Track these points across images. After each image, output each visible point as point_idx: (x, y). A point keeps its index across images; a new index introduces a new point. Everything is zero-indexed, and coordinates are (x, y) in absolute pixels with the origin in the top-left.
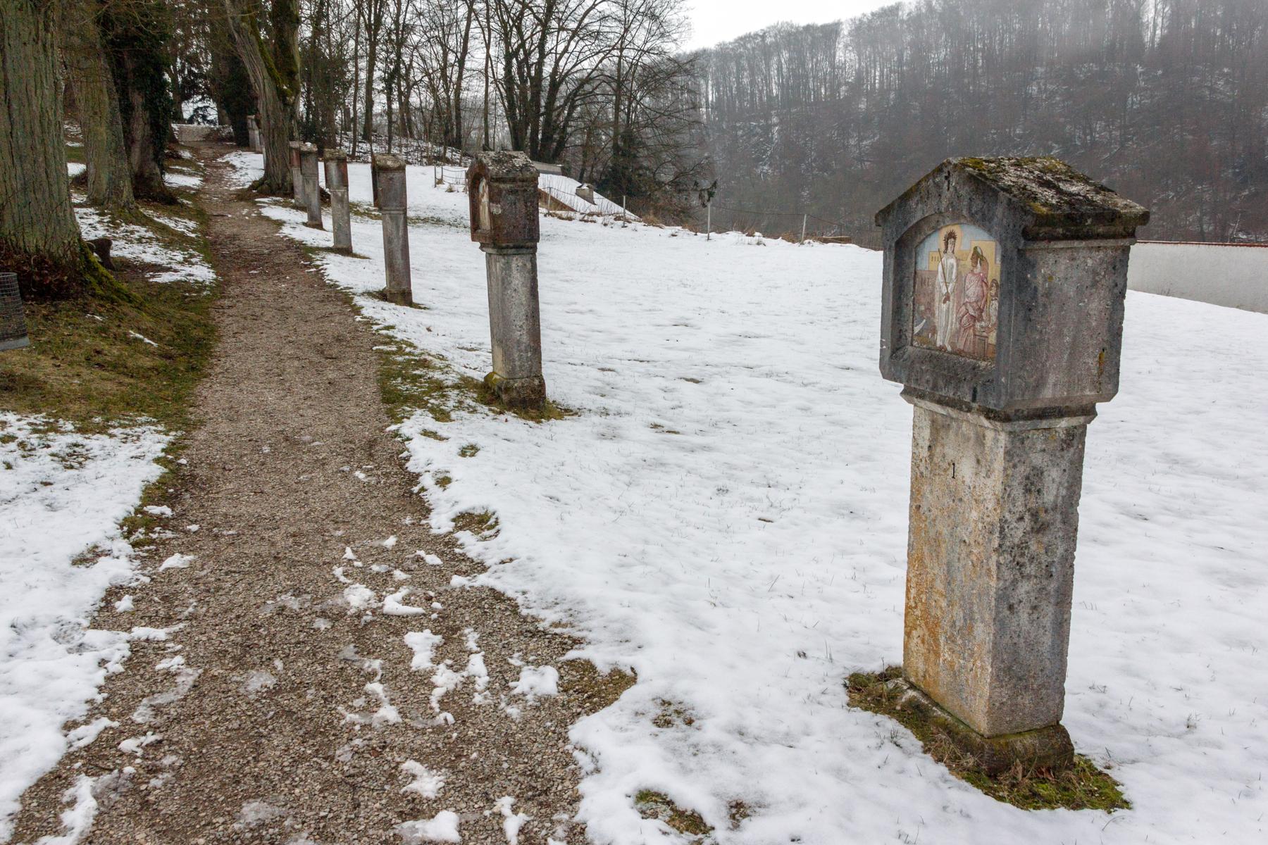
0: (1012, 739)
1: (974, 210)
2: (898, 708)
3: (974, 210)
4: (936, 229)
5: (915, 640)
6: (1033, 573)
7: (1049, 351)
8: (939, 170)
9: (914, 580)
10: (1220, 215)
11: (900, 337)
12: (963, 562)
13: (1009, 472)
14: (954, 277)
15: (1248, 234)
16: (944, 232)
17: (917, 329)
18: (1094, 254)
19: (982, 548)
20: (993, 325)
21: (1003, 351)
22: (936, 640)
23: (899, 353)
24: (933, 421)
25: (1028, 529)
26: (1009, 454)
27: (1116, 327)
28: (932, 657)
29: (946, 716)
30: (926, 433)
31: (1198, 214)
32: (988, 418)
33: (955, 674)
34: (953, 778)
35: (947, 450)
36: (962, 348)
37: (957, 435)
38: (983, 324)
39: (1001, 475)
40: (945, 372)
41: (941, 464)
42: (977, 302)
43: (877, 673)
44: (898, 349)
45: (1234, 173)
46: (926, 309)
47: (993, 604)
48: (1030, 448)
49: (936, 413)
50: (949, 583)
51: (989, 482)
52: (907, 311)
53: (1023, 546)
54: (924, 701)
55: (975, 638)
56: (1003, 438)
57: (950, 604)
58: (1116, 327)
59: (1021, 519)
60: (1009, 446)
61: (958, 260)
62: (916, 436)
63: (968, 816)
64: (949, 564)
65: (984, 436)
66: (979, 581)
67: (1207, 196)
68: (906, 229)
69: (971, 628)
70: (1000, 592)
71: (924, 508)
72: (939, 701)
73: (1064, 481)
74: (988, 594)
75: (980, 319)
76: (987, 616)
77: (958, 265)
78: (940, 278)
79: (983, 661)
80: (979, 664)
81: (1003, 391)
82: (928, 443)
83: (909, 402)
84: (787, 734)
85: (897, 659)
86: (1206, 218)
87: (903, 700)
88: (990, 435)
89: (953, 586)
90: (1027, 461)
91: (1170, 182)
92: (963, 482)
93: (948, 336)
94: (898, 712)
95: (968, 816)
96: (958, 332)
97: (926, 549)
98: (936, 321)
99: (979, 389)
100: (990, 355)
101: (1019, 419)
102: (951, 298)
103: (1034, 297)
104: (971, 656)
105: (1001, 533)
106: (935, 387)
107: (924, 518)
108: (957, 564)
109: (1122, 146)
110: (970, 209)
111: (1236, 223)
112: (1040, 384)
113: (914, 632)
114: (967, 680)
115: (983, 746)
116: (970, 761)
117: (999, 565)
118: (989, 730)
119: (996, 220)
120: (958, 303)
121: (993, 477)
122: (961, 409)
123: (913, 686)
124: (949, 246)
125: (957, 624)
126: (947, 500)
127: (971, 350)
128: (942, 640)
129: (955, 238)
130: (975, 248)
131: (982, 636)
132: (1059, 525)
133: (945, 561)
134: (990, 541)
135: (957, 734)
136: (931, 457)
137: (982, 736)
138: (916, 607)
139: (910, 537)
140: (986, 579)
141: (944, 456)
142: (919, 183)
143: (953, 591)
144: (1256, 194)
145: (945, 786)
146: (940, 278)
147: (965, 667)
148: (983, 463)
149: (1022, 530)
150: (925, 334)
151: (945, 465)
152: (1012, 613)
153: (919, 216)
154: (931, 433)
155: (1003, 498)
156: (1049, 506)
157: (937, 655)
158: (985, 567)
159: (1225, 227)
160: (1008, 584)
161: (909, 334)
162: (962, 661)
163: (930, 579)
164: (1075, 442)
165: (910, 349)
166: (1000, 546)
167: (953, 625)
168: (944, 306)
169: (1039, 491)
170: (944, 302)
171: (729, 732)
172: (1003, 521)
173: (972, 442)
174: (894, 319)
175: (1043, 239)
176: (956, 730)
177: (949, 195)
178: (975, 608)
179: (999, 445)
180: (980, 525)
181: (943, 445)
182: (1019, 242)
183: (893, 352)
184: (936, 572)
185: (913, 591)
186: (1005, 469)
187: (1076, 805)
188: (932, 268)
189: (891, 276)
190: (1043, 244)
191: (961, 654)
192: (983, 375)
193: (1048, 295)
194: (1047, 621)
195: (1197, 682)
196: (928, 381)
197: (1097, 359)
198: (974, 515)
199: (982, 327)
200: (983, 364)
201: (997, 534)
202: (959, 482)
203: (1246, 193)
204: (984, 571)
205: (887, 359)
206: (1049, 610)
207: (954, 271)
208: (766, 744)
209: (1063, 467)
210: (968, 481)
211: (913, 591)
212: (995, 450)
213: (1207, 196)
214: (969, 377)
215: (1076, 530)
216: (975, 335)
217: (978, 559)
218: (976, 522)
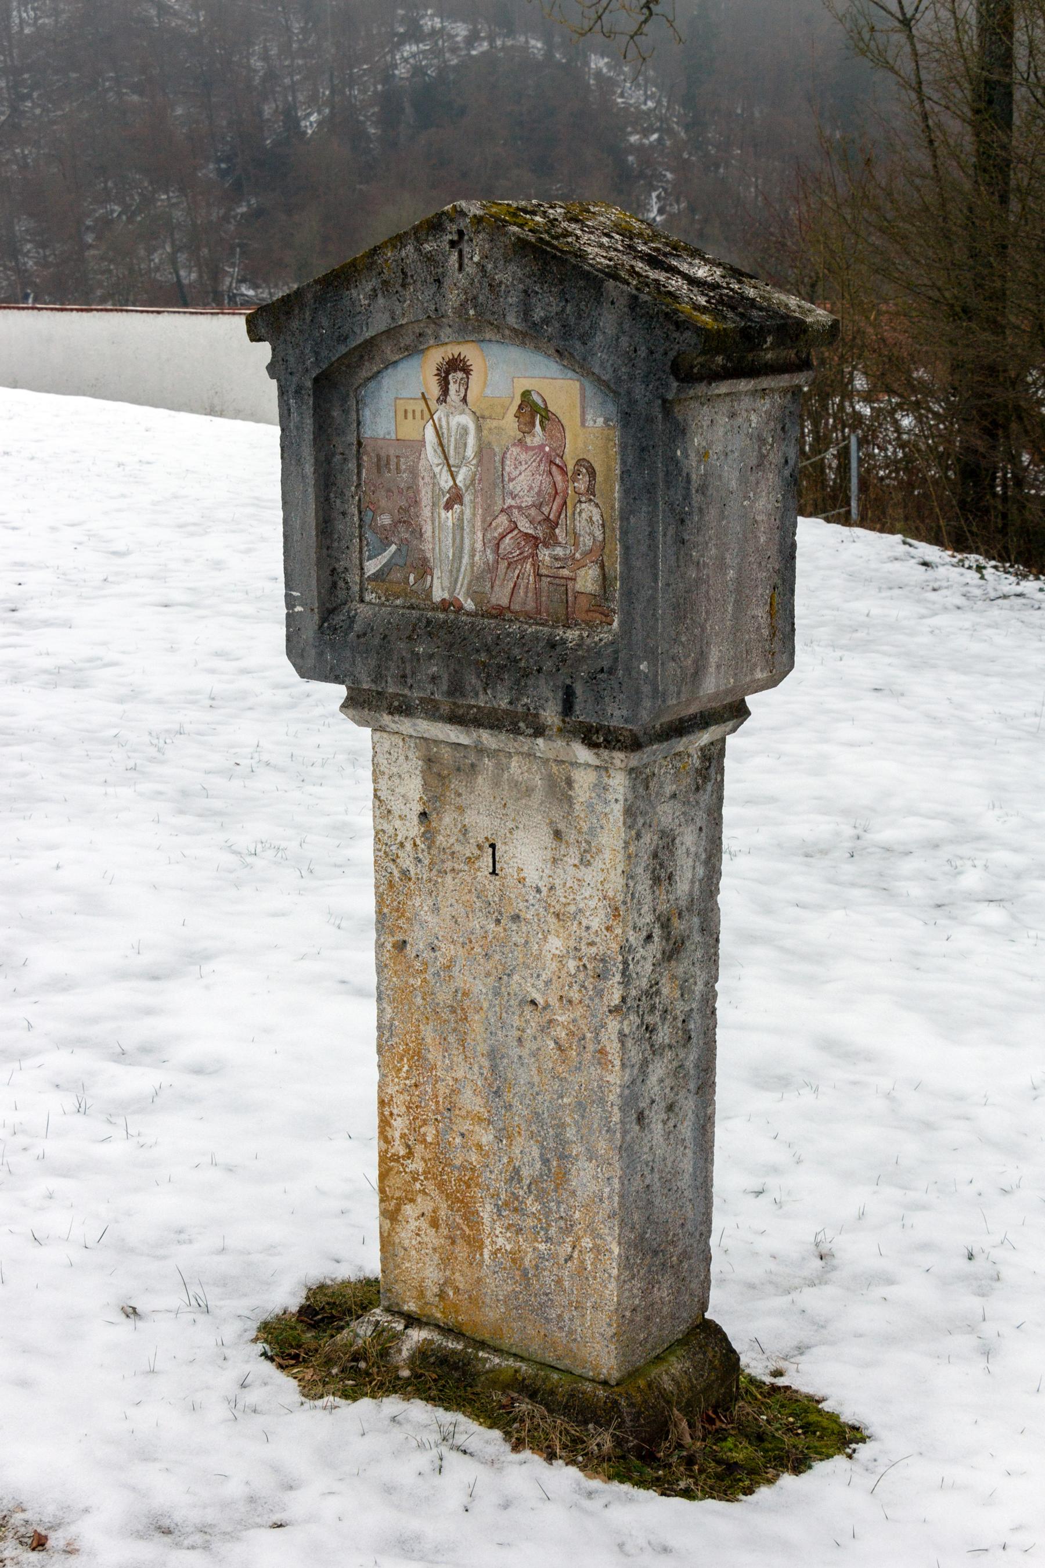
0: (654, 1372)
1: (538, 314)
2: (405, 1373)
3: (538, 314)
4: (414, 350)
5: (413, 1224)
6: (667, 1041)
7: (709, 600)
8: (435, 226)
9: (401, 1099)
10: (205, 251)
11: (334, 585)
12: (530, 1045)
13: (632, 849)
14: (470, 452)
15: (255, 286)
16: (436, 356)
17: (372, 567)
18: (759, 403)
19: (580, 1011)
20: (585, 554)
21: (639, 607)
22: (471, 1217)
23: (338, 619)
24: (429, 761)
25: (659, 956)
26: (629, 812)
27: (789, 541)
28: (461, 1251)
29: (511, 1362)
30: (413, 787)
31: (169, 249)
32: (592, 745)
33: (525, 1274)
34: (596, 1484)
35: (470, 818)
36: (504, 602)
37: (496, 784)
38: (559, 551)
39: (620, 856)
40: (483, 657)
41: (457, 847)
42: (539, 506)
43: (294, 1309)
44: (332, 611)
45: (219, 170)
46: (395, 524)
47: (616, 1117)
48: (657, 793)
49: (437, 742)
50: (497, 1093)
51: (589, 875)
52: (346, 526)
53: (652, 991)
54: (452, 1345)
55: (573, 1193)
56: (618, 783)
57: (504, 1134)
58: (789, 543)
59: (649, 937)
60: (630, 796)
61: (479, 419)
62: (383, 795)
63: (666, 1550)
64: (493, 1055)
65: (569, 782)
66: (580, 1078)
67: (178, 215)
68: (343, 349)
69: (562, 1178)
70: (627, 1092)
71: (418, 941)
72: (487, 1337)
73: (701, 849)
74: (602, 1101)
75: (550, 540)
76: (602, 1146)
77: (479, 429)
78: (431, 454)
79: (595, 1235)
80: (587, 1242)
81: (646, 689)
82: (418, 808)
83: (362, 722)
84: (252, 1500)
85: (371, 1265)
86: (182, 257)
87: (405, 1354)
88: (584, 780)
89: (507, 1097)
90: (654, 823)
91: (110, 184)
92: (521, 881)
93: (463, 580)
94: (408, 1381)
95: (666, 1550)
96: (491, 569)
97: (428, 1032)
98: (427, 546)
99: (579, 689)
100: (580, 616)
101: (651, 742)
102: (467, 498)
103: (687, 496)
104: (568, 1230)
105: (623, 974)
106: (456, 689)
107: (417, 965)
108: (515, 1052)
109: (14, 109)
110: (526, 313)
111: (233, 265)
112: (698, 673)
113: (408, 1209)
114: (559, 1282)
115: (615, 1402)
116: (603, 1440)
117: (622, 1036)
118: (619, 1370)
119: (599, 338)
120: (487, 510)
121: (598, 864)
122: (516, 731)
123: (412, 1321)
124: (453, 387)
125: (525, 1172)
126: (478, 923)
127: (531, 605)
128: (486, 1212)
129: (467, 371)
130: (526, 394)
131: (593, 1187)
132: (697, 937)
133: (483, 1048)
134: (600, 993)
135: (552, 1393)
136: (429, 836)
137: (605, 1383)
138: (410, 1154)
139: (381, 1011)
140: (595, 1072)
141: (465, 831)
142: (375, 251)
143: (509, 1107)
144: (258, 213)
145: (595, 1505)
146: (431, 454)
147: (554, 1256)
148: (571, 836)
149: (650, 960)
150: (396, 575)
151: (470, 850)
152: (642, 1128)
153: (379, 323)
154: (425, 785)
155: (625, 903)
156: (683, 903)
157: (475, 1244)
158: (591, 1047)
159: (216, 275)
160: (636, 1071)
161: (354, 578)
162: (542, 1247)
163: (442, 1089)
164: (712, 770)
165: (361, 608)
166: (624, 999)
167: (516, 1175)
168: (448, 517)
169: (670, 877)
170: (448, 506)
171: (140, 1535)
172: (626, 949)
173: (538, 796)
174: (320, 547)
175: (700, 379)
176: (548, 1386)
177: (463, 282)
178: (570, 1133)
179: (610, 797)
180: (572, 965)
181: (461, 809)
182: (667, 386)
183: (323, 620)
184: (460, 1074)
185: (399, 1125)
186: (627, 844)
187: (799, 1465)
188: (408, 430)
189: (307, 452)
190: (701, 389)
191: (541, 1232)
192: (581, 660)
193: (703, 489)
194: (687, 1130)
195: (775, 1170)
196: (434, 679)
197: (768, 608)
198: (555, 944)
199: (557, 559)
200: (572, 635)
201: (618, 978)
202: (511, 882)
203: (243, 209)
204: (588, 1056)
205: (309, 632)
206: (688, 1104)
207: (471, 440)
208: (229, 1536)
209: (699, 824)
210: (532, 877)
211: (399, 1125)
212: (599, 808)
213: (178, 215)
214: (548, 665)
215: (717, 940)
216: (538, 575)
217: (571, 1034)
218: (560, 959)
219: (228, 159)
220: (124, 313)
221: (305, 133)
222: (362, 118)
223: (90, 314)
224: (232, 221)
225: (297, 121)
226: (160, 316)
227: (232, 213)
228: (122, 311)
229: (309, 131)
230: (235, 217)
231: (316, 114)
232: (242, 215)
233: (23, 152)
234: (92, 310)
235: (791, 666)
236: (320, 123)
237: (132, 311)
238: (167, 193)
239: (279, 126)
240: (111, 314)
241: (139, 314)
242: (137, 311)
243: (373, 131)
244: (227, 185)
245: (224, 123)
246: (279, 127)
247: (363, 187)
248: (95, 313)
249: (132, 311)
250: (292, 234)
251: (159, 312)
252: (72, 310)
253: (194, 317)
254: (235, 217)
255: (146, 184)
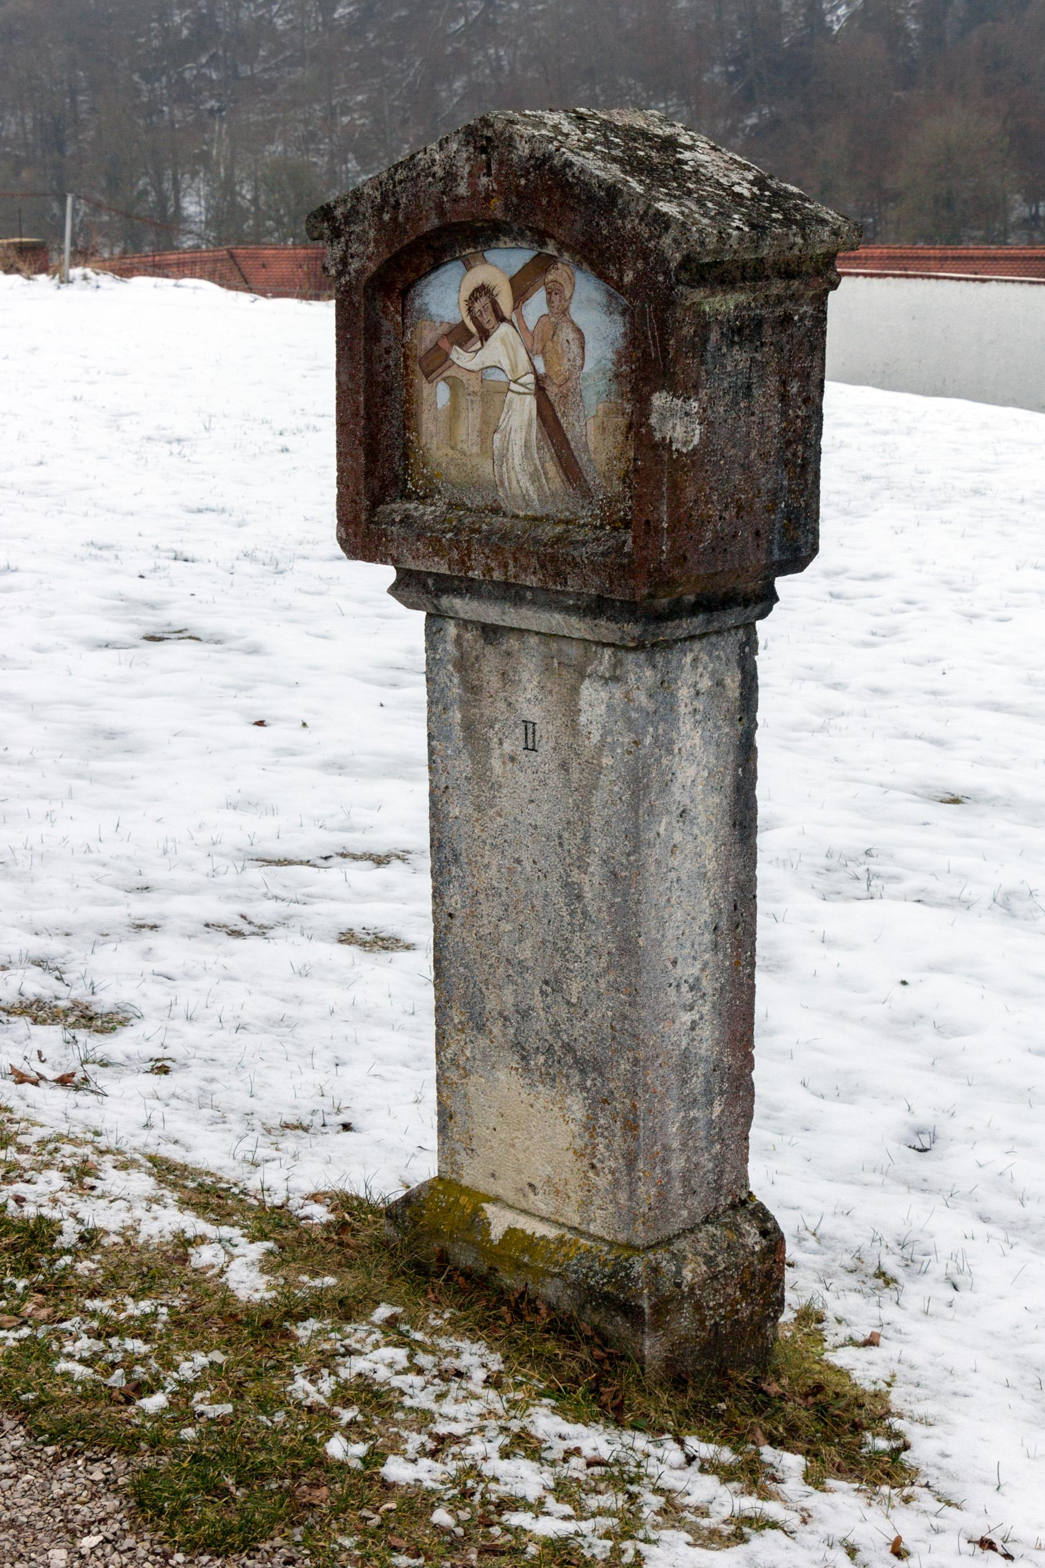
91: (598, 90)
144: (775, 123)
203: (752, 121)
219: (737, 61)
220: (933, 281)
221: (831, 29)
222: (900, 11)
223: (882, 281)
224: (740, 134)
225: (821, 15)
226: (986, 285)
227: (741, 125)
228: (930, 277)
229: (836, 28)
230: (743, 129)
231: (844, 7)
232: (753, 127)
233: (497, 53)
234: (886, 275)
235: (815, 550)
236: (850, 18)
237: (945, 278)
238: (666, 101)
239: (799, 21)
240: (913, 281)
241: (954, 283)
242: (952, 278)
243: (913, 27)
244: (735, 91)
245: (734, 17)
246: (800, 22)
247: (900, 94)
248: (890, 279)
249: (945, 278)
250: (814, 151)
251: (983, 281)
252: (857, 275)
253: (1035, 288)
254: (743, 129)
255: (639, 90)
